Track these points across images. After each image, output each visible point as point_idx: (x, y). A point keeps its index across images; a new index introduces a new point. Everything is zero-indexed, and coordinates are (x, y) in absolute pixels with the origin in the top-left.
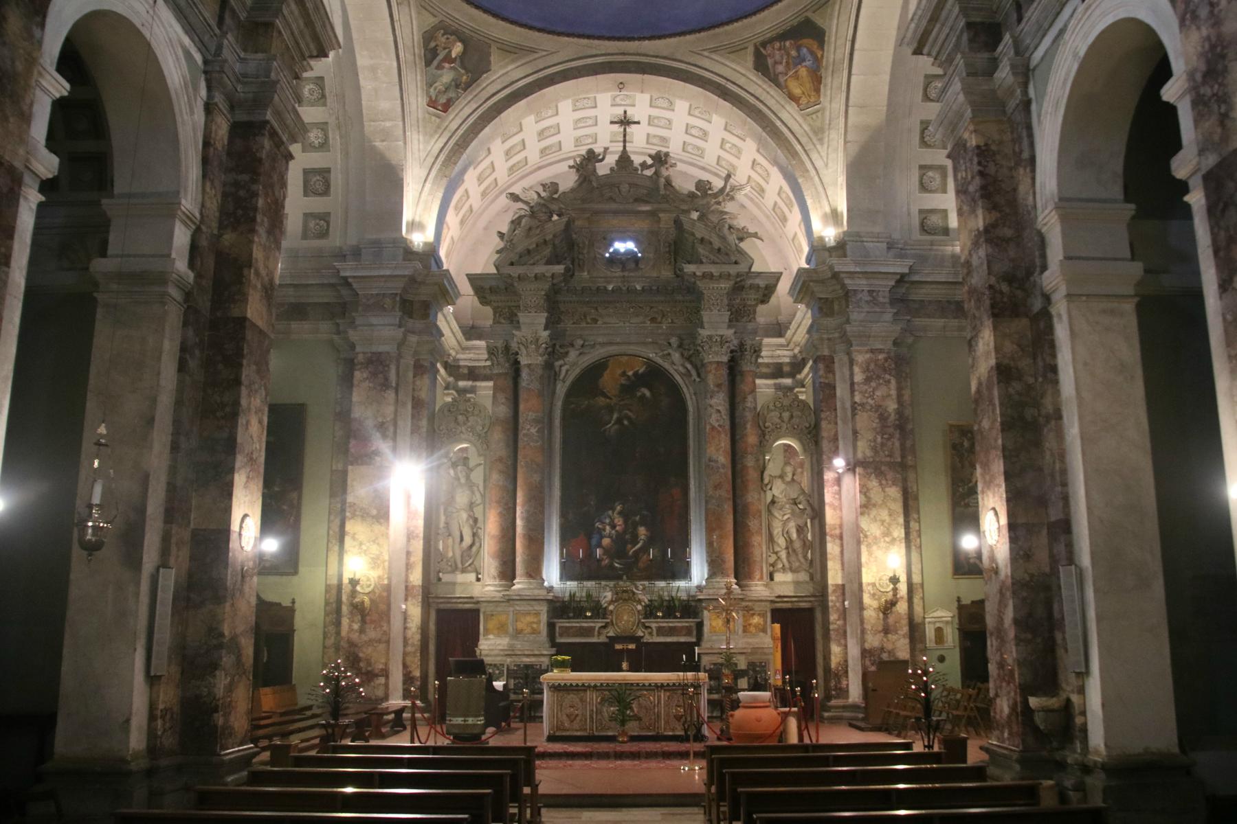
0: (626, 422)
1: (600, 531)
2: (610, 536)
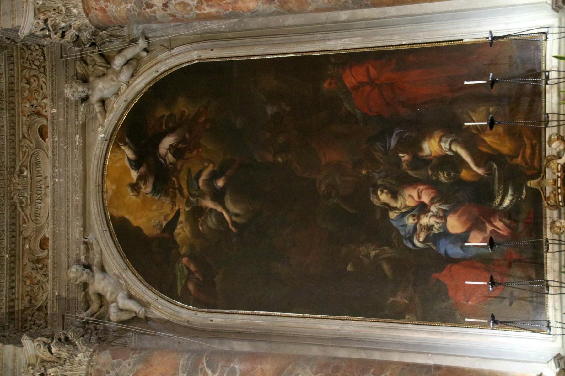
0: (220, 183)
1: (433, 238)
2: (444, 216)
